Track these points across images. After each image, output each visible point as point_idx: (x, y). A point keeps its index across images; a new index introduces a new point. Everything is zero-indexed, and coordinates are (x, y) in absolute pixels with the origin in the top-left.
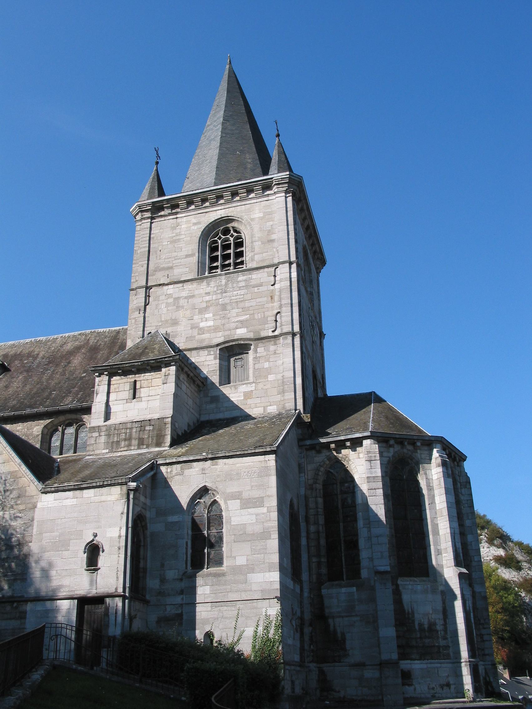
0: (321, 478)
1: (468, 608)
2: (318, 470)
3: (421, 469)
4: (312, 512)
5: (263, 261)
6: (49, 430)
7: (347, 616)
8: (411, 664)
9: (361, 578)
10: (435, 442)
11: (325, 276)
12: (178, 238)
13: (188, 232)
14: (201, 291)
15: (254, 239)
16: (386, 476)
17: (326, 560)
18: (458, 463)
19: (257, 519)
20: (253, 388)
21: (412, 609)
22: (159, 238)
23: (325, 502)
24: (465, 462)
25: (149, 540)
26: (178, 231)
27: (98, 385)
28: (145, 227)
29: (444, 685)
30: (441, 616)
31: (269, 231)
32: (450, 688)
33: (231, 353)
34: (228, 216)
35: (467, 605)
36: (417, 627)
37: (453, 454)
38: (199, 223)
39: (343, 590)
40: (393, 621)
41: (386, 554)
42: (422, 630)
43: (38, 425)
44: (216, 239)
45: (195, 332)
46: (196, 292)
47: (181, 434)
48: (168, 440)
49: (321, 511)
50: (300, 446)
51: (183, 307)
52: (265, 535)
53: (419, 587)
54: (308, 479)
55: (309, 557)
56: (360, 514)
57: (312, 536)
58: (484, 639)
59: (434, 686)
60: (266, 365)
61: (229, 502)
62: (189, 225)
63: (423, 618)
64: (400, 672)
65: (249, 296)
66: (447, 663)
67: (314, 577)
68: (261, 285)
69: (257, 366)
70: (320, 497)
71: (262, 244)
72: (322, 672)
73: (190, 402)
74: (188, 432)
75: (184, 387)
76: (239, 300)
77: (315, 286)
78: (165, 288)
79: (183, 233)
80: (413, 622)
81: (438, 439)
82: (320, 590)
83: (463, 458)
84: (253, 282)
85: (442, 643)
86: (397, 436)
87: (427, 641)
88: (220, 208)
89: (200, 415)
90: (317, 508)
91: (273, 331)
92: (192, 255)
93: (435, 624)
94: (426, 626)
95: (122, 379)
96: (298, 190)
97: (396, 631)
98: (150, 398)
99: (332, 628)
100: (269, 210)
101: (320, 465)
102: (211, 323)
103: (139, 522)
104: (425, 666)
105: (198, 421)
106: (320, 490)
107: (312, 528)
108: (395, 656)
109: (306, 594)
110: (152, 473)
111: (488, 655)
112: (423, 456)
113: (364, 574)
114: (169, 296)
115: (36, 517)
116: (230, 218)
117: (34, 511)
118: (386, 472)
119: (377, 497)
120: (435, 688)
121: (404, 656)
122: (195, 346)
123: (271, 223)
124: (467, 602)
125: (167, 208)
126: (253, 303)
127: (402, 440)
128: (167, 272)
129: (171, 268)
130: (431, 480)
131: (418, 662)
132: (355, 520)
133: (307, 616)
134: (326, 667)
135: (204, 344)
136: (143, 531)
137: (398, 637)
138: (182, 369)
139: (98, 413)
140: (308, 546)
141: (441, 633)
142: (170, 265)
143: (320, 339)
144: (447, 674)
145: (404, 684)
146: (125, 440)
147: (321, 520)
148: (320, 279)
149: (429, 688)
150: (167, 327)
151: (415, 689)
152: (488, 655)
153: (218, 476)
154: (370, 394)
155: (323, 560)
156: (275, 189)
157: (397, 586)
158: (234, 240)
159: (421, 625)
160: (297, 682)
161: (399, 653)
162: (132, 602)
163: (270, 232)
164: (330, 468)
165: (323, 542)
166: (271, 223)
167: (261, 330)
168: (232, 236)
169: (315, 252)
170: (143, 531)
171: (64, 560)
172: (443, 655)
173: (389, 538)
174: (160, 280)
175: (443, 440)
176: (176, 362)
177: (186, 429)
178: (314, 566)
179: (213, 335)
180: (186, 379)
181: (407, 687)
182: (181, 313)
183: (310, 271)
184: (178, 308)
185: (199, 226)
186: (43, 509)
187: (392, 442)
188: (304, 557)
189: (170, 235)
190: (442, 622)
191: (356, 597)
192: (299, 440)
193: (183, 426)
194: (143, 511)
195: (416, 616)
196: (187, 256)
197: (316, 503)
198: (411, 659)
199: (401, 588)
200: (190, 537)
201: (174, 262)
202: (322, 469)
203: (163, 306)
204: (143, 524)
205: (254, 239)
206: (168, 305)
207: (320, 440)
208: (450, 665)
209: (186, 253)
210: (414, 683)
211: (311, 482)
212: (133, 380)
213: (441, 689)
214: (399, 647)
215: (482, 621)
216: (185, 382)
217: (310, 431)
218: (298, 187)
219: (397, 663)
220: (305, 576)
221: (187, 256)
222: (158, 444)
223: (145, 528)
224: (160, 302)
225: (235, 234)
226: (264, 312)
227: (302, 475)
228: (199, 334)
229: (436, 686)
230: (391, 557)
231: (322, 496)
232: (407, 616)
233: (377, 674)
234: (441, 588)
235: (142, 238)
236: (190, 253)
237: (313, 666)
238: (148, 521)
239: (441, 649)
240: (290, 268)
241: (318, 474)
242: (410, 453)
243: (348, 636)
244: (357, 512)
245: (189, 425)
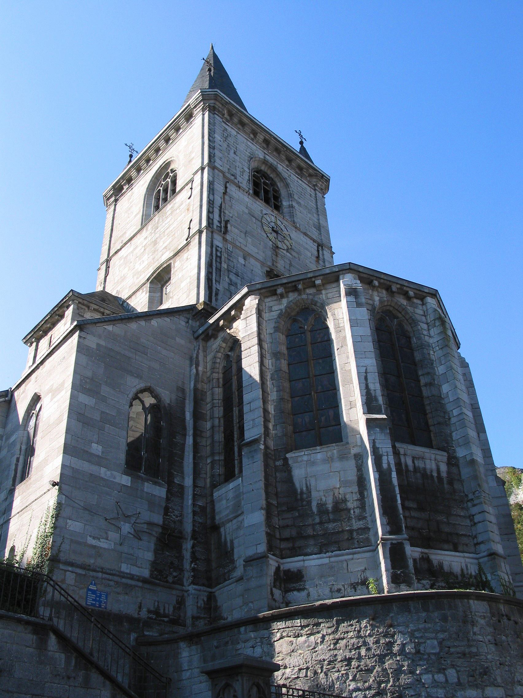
1: (385, 466)
3: (328, 310)
8: (304, 561)
10: (341, 272)
21: (307, 487)
29: (357, 584)
30: (355, 489)
33: (163, 283)
34: (164, 162)
36: (315, 509)
53: (319, 456)
58: (476, 521)
59: (340, 587)
63: (325, 496)
80: (309, 503)
81: (345, 268)
85: (356, 525)
87: (331, 526)
93: (345, 501)
104: (326, 561)
111: (482, 542)
112: (330, 295)
116: (166, 162)
119: (252, 356)
120: (343, 589)
124: (384, 459)
125: (125, 185)
127: (293, 284)
130: (342, 319)
141: (354, 512)
144: (363, 568)
148: (326, 200)
152: (482, 542)
159: (321, 505)
162: (208, 593)
172: (358, 541)
173: (275, 404)
175: (352, 266)
176: (73, 300)
190: (356, 496)
195: (314, 494)
199: (290, 462)
202: (219, 355)
207: (209, 321)
210: (307, 587)
213: (353, 590)
215: (471, 496)
229: (343, 586)
230: (278, 426)
232: (299, 497)
234: (354, 451)
239: (355, 534)
242: (311, 297)
243: (236, 542)
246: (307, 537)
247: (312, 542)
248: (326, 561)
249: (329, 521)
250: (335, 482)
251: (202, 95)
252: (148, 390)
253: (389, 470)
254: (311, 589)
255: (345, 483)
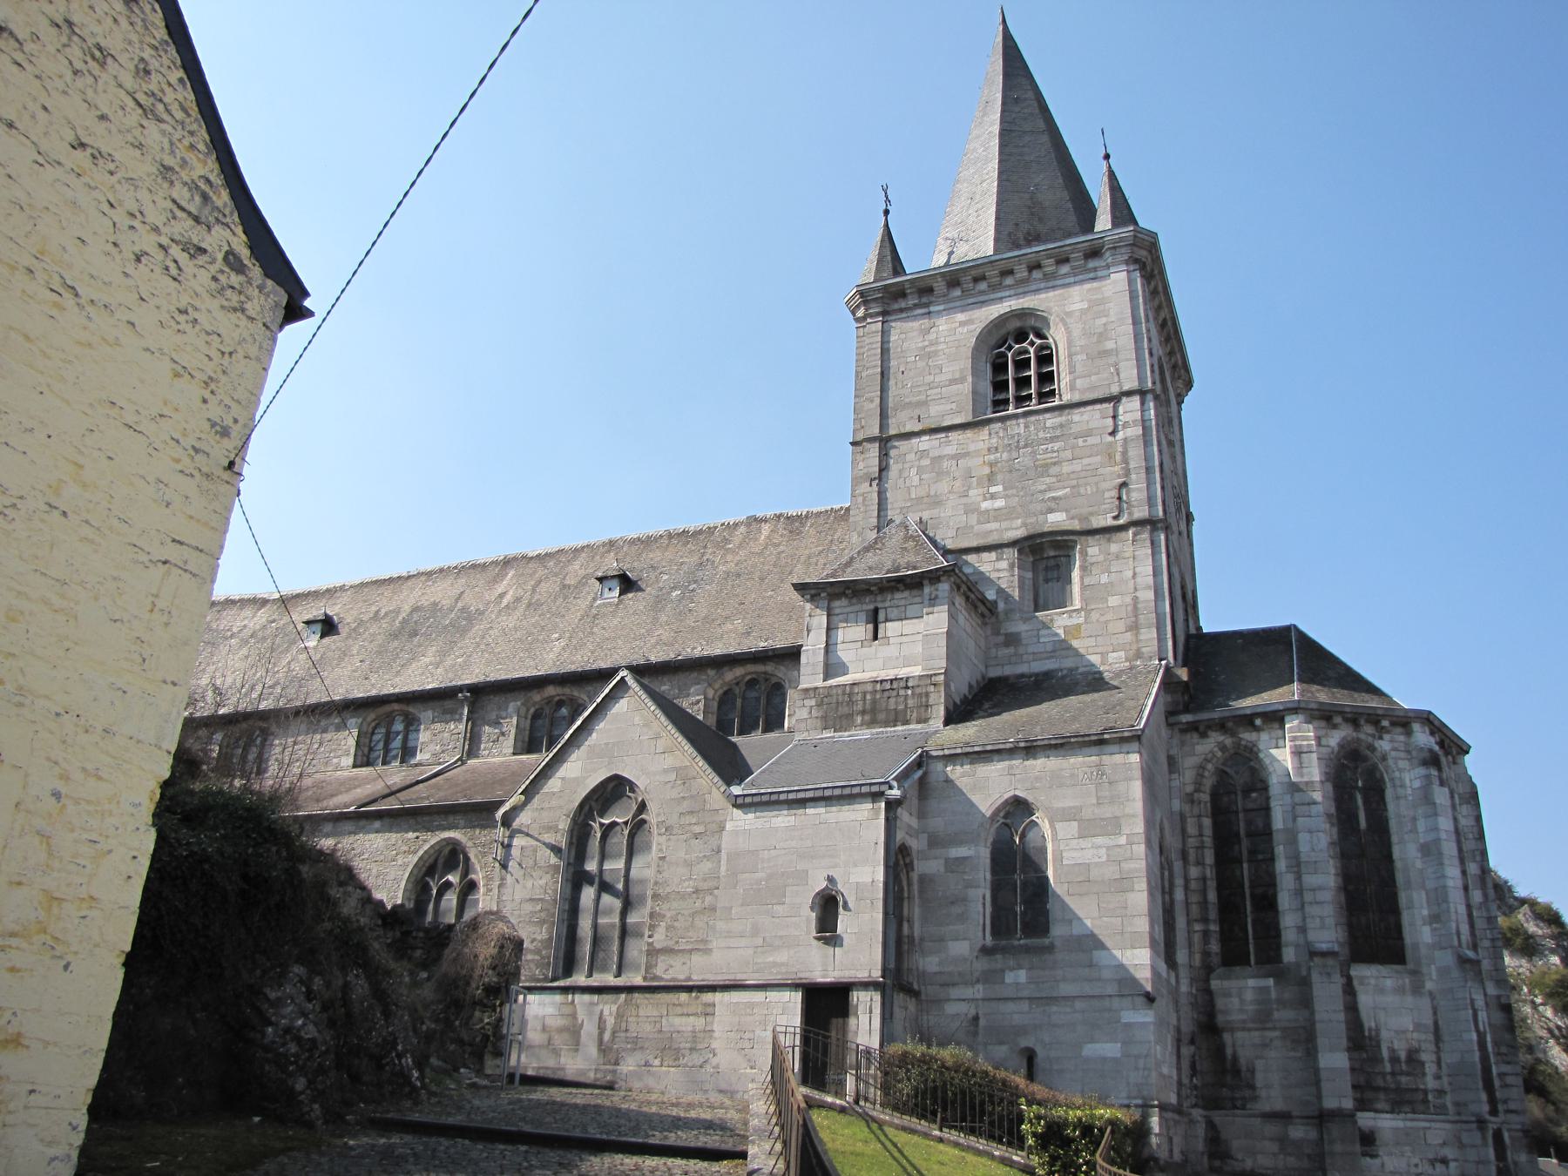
0: (1208, 783)
2: (1202, 767)
4: (1192, 842)
5: (1093, 388)
6: (716, 691)
7: (1257, 1029)
9: (1281, 962)
11: (1192, 408)
12: (933, 349)
13: (952, 338)
14: (981, 445)
15: (1073, 349)
16: (1327, 780)
17: (1218, 929)
18: (1454, 758)
19: (1108, 855)
20: (1081, 620)
22: (899, 350)
23: (1216, 825)
24: (1467, 757)
25: (916, 887)
26: (932, 336)
27: (810, 616)
28: (874, 329)
30: (1431, 1037)
31: (1101, 334)
32: (1447, 1167)
35: (1480, 1018)
37: (1447, 742)
38: (969, 322)
39: (1251, 982)
40: (1344, 1042)
41: (1330, 921)
42: (1395, 1060)
43: (698, 684)
44: (1002, 349)
45: (973, 519)
46: (972, 448)
47: (958, 702)
48: (940, 712)
49: (1208, 841)
50: (1170, 725)
51: (948, 473)
52: (1122, 884)
54: (1184, 784)
55: (1189, 923)
56: (1281, 847)
57: (1193, 885)
60: (1104, 579)
61: (1058, 826)
62: (953, 326)
64: (1357, 1133)
65: (1068, 454)
66: (1444, 1121)
67: (1197, 957)
68: (1088, 433)
69: (1087, 581)
70: (1207, 817)
71: (1088, 358)
72: (1211, 1125)
73: (971, 644)
74: (970, 697)
75: (961, 619)
76: (1049, 461)
77: (1176, 428)
78: (915, 441)
79: (942, 340)
80: (1379, 1046)
82: (1207, 980)
83: (1464, 749)
84: (1075, 429)
86: (1348, 710)
87: (1404, 1079)
88: (1007, 293)
89: (986, 667)
90: (1201, 835)
91: (1116, 518)
92: (962, 380)
94: (1403, 1055)
95: (852, 605)
96: (1149, 259)
97: (1350, 1059)
98: (904, 639)
99: (1229, 1051)
100: (1099, 296)
101: (1206, 760)
102: (1000, 503)
103: (900, 857)
104: (1400, 1124)
105: (983, 678)
106: (1206, 802)
107: (1194, 872)
108: (1348, 1104)
109: (1184, 988)
110: (920, 773)
113: (1289, 955)
114: (923, 454)
115: (723, 846)
117: (720, 838)
118: (1326, 773)
121: (1363, 1105)
122: (974, 544)
123: (1104, 320)
126: (1077, 466)
128: (917, 412)
129: (925, 403)
131: (1388, 1116)
132: (1272, 859)
133: (1187, 1028)
134: (1218, 1117)
135: (990, 540)
136: (908, 873)
137: (1353, 1069)
138: (959, 588)
139: (813, 665)
140: (1187, 904)
142: (923, 397)
143: (1188, 525)
145: (1365, 1154)
146: (863, 712)
147: (1209, 858)
149: (1409, 1166)
150: (922, 511)
151: (1383, 1165)
153: (1037, 779)
154: (1287, 630)
155: (1214, 927)
156: (1108, 257)
157: (1349, 979)
158: (1035, 352)
159: (1392, 1050)
160: (1176, 1140)
161: (1355, 1099)
163: (1102, 337)
164: (1223, 764)
165: (1212, 896)
166: (1104, 320)
167: (1092, 514)
168: (1032, 344)
169: (1174, 367)
170: (908, 873)
171: (777, 920)
174: (904, 426)
177: (967, 694)
178: (1197, 938)
179: (1005, 524)
180: (964, 604)
181: (1368, 1159)
182: (943, 487)
183: (1168, 402)
184: (940, 474)
185: (972, 327)
186: (736, 833)
187: (1338, 720)
188: (1181, 922)
189: (920, 345)
191: (1273, 995)
192: (1171, 713)
193: (961, 688)
194: (907, 837)
196: (953, 382)
197: (1200, 827)
198: (1376, 1111)
199: (1355, 983)
200: (988, 885)
201: (929, 393)
202: (1210, 766)
203: (913, 471)
204: (907, 861)
205: (1073, 349)
206: (920, 470)
208: (1448, 1126)
209: (950, 377)
210: (1381, 1153)
211: (1189, 789)
212: (871, 607)
214: (1354, 1087)
216: (963, 611)
217: (1186, 698)
218: (1150, 252)
219: (1352, 1116)
220: (1181, 956)
221: (953, 382)
222: (923, 720)
223: (909, 867)
224: (907, 466)
225: (1038, 342)
226: (1097, 484)
227: (1175, 776)
228: (979, 522)
229: (1421, 1160)
231: (1209, 814)
233: (1313, 1134)
235: (869, 350)
236: (957, 376)
237: (1197, 1113)
238: (914, 854)
240: (1143, 403)
241: (1202, 776)
244: (1275, 844)
245: (970, 686)
246: (1377, 1089)
247: (1382, 1096)
248: (1400, 1124)
249: (1402, 1073)
250: (1407, 1022)
251: (1135, 236)
252: (871, 480)
253: (1485, 1033)
254: (1385, 1158)
255: (1418, 1027)
